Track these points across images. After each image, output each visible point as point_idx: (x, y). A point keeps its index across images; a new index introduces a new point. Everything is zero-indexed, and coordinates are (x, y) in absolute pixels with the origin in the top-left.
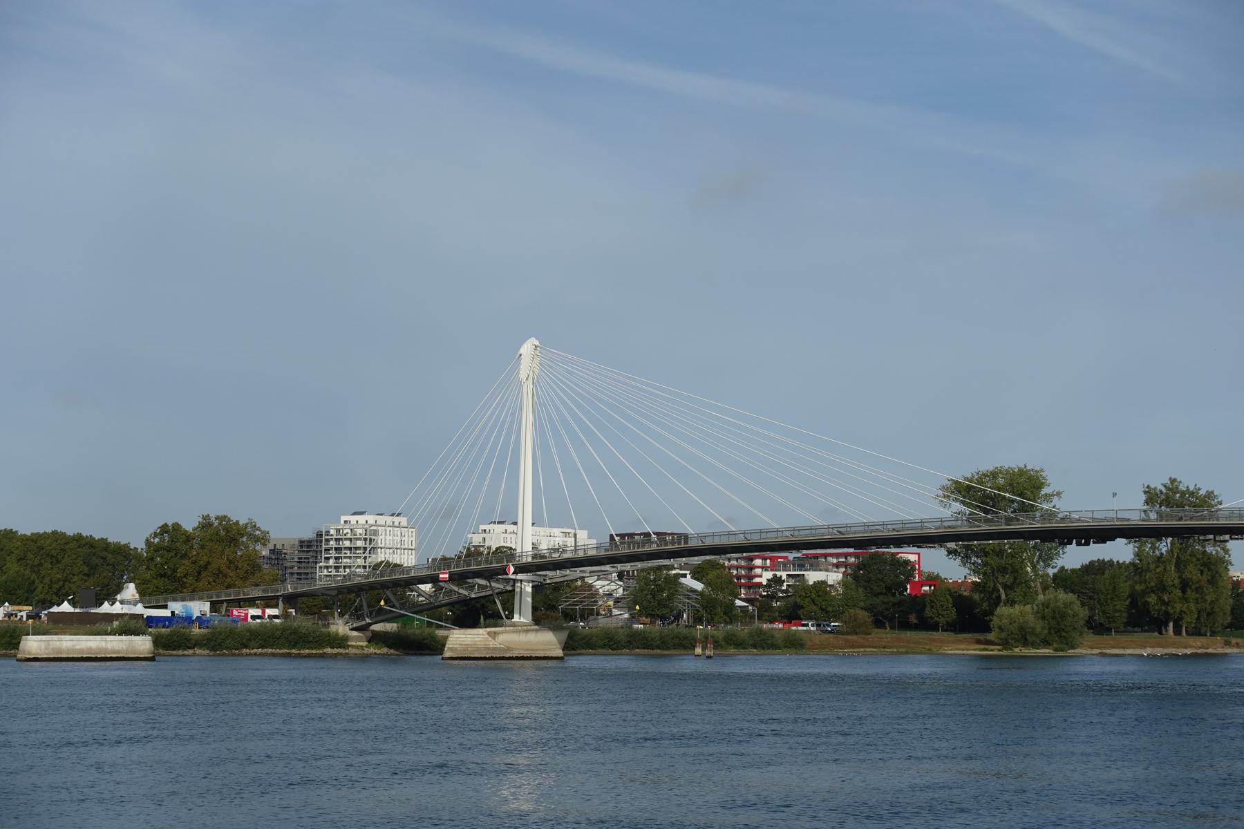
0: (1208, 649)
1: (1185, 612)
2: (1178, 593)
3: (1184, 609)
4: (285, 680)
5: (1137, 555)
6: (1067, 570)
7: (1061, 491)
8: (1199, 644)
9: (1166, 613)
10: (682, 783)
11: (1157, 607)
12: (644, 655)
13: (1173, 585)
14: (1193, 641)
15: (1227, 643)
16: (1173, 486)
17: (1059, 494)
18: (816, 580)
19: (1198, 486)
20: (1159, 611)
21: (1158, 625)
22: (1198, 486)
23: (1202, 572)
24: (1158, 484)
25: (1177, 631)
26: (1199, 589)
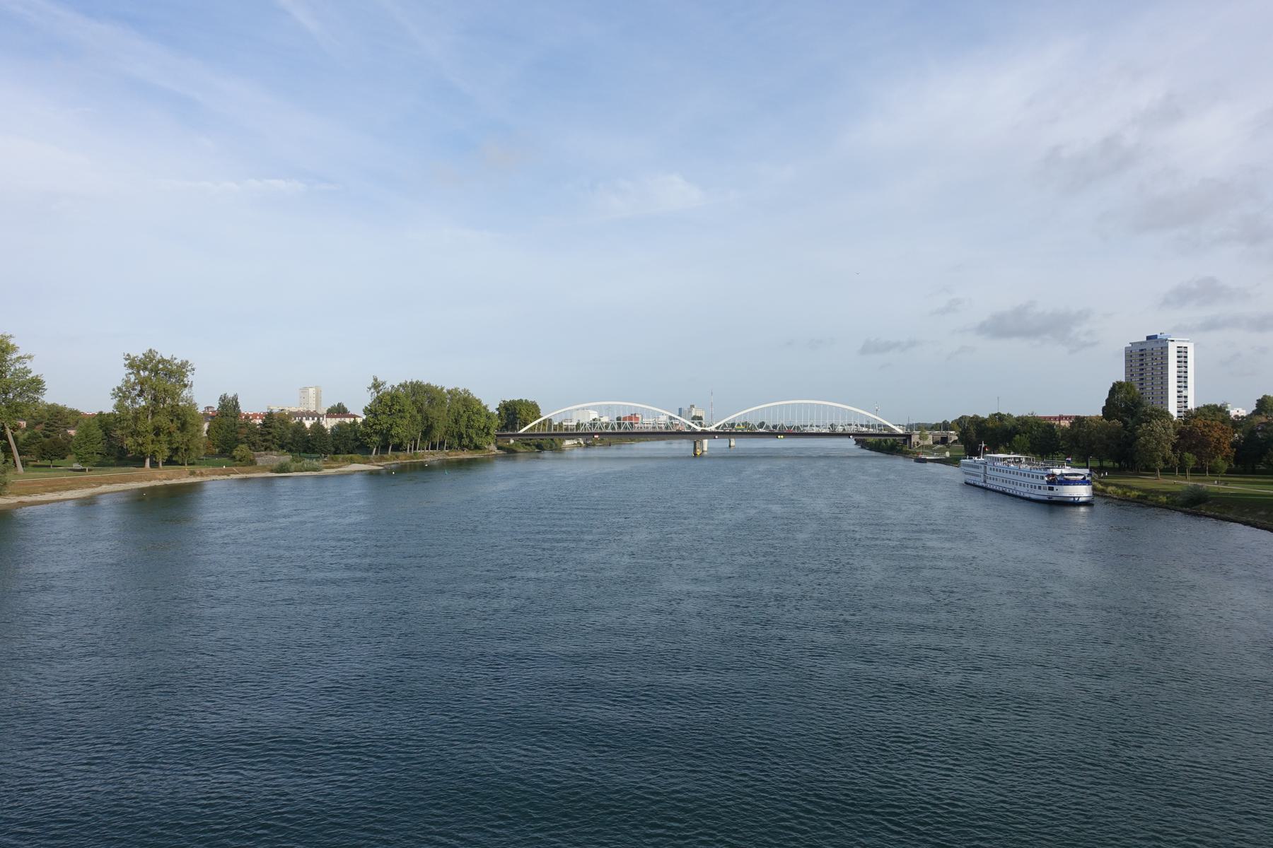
0: (171, 479)
1: (158, 452)
2: (152, 436)
3: (156, 449)
4: (904, 511)
5: (116, 407)
6: (104, 415)
7: (32, 354)
8: (164, 476)
9: (141, 453)
10: (942, 594)
11: (133, 447)
12: (875, 457)
13: (147, 431)
14: (171, 470)
15: (193, 473)
16: (150, 356)
17: (30, 357)
18: (1115, 381)
19: (174, 356)
20: (136, 450)
21: (138, 461)
22: (174, 356)
23: (172, 421)
24: (138, 353)
25: (154, 464)
26: (170, 434)
